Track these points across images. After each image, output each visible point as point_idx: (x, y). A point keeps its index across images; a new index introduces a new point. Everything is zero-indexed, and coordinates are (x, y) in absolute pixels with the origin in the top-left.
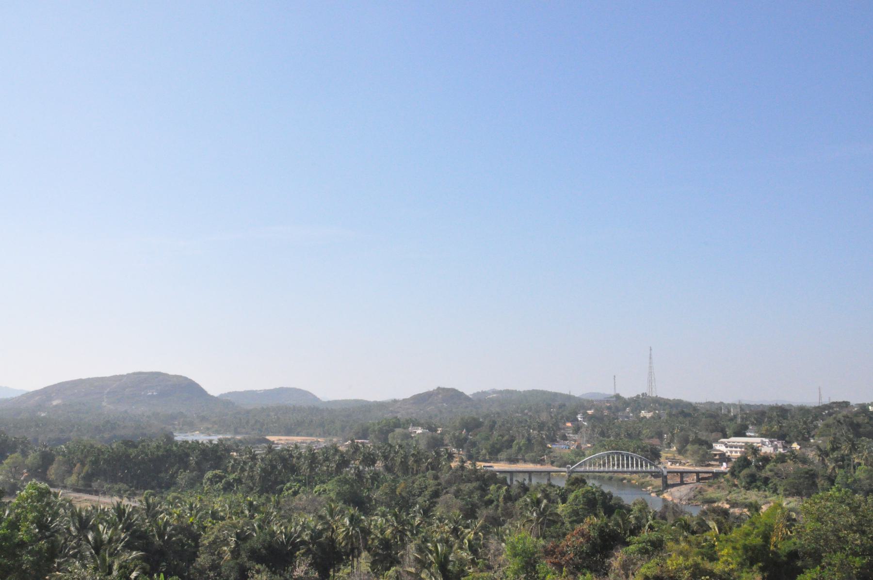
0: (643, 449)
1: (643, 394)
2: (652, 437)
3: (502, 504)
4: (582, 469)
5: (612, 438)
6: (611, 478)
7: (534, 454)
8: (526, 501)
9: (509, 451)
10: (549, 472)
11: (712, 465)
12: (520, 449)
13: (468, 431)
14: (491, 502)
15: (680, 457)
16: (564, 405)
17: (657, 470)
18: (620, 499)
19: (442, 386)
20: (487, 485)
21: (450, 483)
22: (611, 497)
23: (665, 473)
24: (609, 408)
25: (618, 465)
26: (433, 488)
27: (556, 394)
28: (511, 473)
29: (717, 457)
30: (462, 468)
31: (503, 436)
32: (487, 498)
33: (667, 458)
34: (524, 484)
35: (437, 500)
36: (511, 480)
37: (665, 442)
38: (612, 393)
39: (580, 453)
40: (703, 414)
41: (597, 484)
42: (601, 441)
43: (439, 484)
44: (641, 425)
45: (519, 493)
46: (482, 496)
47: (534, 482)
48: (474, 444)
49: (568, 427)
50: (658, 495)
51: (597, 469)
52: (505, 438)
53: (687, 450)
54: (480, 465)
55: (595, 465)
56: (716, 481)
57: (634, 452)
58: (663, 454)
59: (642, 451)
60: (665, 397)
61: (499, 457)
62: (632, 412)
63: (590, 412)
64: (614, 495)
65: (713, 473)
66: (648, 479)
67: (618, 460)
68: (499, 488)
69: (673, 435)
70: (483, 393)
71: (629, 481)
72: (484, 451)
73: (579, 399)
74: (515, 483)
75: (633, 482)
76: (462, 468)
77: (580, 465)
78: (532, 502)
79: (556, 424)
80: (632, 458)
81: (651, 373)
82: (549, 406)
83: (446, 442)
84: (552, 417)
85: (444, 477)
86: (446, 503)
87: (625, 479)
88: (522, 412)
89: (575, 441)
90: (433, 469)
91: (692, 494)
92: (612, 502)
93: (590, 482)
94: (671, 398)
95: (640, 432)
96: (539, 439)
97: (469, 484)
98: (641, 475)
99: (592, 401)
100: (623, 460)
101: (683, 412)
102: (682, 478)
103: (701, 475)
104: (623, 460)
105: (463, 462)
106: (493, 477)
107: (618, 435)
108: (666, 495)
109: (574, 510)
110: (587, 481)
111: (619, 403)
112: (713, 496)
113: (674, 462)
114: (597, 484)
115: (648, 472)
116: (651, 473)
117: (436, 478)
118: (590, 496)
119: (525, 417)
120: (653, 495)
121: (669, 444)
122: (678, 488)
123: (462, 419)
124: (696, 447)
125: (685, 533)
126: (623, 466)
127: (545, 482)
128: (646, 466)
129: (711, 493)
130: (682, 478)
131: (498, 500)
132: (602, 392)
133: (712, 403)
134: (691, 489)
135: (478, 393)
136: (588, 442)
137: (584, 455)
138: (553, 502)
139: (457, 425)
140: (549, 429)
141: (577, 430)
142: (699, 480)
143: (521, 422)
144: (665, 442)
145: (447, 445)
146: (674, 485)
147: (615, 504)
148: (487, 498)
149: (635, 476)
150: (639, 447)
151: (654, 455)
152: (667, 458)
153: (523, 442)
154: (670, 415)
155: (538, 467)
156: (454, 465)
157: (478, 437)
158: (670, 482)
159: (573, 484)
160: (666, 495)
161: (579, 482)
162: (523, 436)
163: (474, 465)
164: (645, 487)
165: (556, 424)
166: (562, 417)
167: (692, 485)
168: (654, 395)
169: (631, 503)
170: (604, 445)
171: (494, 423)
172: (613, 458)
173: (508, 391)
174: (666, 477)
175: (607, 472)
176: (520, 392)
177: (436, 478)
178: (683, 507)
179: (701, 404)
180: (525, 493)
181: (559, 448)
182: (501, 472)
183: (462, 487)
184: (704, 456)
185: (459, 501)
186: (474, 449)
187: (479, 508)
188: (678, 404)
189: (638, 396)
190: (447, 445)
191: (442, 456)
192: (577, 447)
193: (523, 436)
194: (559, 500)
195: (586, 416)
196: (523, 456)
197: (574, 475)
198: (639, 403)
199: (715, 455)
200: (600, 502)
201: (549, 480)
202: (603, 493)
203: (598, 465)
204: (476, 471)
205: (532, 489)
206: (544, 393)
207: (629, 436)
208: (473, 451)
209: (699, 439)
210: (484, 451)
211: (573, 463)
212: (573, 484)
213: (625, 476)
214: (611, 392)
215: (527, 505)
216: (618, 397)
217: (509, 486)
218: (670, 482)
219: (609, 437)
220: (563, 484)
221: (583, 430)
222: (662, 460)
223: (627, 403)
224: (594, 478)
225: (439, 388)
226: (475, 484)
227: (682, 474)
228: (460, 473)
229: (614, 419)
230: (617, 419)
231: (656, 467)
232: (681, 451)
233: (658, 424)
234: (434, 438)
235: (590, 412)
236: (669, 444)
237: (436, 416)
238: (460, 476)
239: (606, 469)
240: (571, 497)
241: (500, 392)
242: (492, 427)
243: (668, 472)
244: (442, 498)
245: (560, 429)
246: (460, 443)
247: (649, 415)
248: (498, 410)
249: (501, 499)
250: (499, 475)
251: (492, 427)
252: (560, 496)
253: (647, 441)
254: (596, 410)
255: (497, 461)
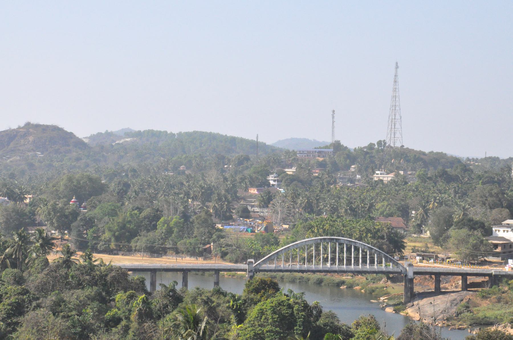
0: (376, 235)
1: (379, 143)
2: (391, 215)
3: (134, 325)
4: (273, 266)
5: (324, 216)
6: (319, 282)
7: (192, 241)
8: (176, 319)
9: (151, 234)
10: (217, 271)
11: (490, 263)
12: (170, 231)
13: (80, 200)
14: (116, 321)
15: (437, 248)
16: (247, 159)
17: (396, 269)
18: (333, 316)
19: (34, 121)
20: (109, 293)
21: (44, 289)
22: (320, 312)
23: (410, 275)
24: (322, 165)
25: (333, 260)
26: (13, 299)
27: (233, 140)
28: (154, 271)
29: (499, 250)
30: (67, 263)
31: (140, 210)
32: (109, 314)
33: (414, 250)
34: (173, 290)
35: (21, 319)
36: (153, 284)
37: (413, 222)
38: (329, 140)
39: (270, 239)
40: (480, 177)
41: (297, 291)
42: (306, 220)
43: (26, 292)
44: (373, 194)
45: (166, 306)
46: (101, 312)
47: (192, 287)
48: (89, 223)
49: (251, 196)
50: (397, 311)
51: (298, 267)
52: (147, 212)
53: (448, 237)
54: (98, 258)
55: (293, 260)
56: (495, 288)
57: (360, 239)
58: (409, 244)
59: (373, 237)
60: (417, 148)
61: (133, 244)
62: (360, 171)
63: (290, 171)
64: (325, 310)
65: (490, 275)
66: (381, 283)
67: (334, 252)
68: (132, 297)
69: (426, 211)
70: (109, 134)
71: (350, 287)
72: (107, 235)
73: (272, 149)
74: (158, 288)
75: (357, 288)
76: (67, 263)
77: (270, 260)
78: (187, 321)
79: (232, 191)
80: (357, 249)
81: (394, 108)
82: (221, 160)
83: (40, 217)
84: (225, 179)
85: (35, 278)
86: (37, 324)
87: (343, 283)
88: (175, 169)
89: (263, 219)
90: (14, 265)
91: (454, 310)
92: (321, 322)
93: (285, 288)
94: (427, 151)
95: (372, 206)
96: (203, 214)
97: (79, 291)
98: (370, 277)
99: (294, 153)
100: (342, 251)
101: (446, 172)
102: (438, 282)
103: (471, 280)
104: (342, 251)
105: (69, 253)
106: (120, 278)
107: (334, 210)
108: (411, 312)
109: (256, 335)
110: (281, 286)
111: (338, 157)
112: (489, 314)
113: (425, 256)
114: (297, 291)
115: (382, 272)
116: (386, 273)
117: (19, 281)
118: (285, 311)
119: (181, 178)
120: (389, 310)
121: (419, 226)
122: (431, 299)
123: (70, 179)
124: (465, 231)
125: (396, 238)
126: (341, 261)
127: (210, 287)
128: (380, 262)
129: (486, 309)
130: (438, 282)
131: (128, 318)
132: (311, 138)
133: (494, 160)
134: (452, 302)
135: (99, 134)
136: (284, 221)
137: (277, 243)
138: (222, 321)
139: (62, 188)
140: (220, 199)
141: (267, 201)
142: (466, 287)
143: (172, 187)
144: (413, 222)
145: (41, 224)
146: (423, 295)
147: (325, 325)
148: (109, 314)
149: (361, 279)
150: (368, 231)
151: (395, 244)
152: (414, 250)
153: (175, 219)
154: (424, 178)
155: (199, 263)
156: (52, 257)
157: (97, 211)
158: (417, 289)
159: (257, 291)
160: (411, 312)
161: (268, 287)
162: (176, 210)
163: (89, 257)
164: (377, 297)
165: (232, 191)
166: (243, 180)
167: (453, 296)
168: (398, 145)
169: (352, 324)
170: (311, 227)
171: (127, 186)
172: (325, 249)
173: (152, 134)
174: (411, 281)
175: (314, 272)
176: (173, 135)
177: (19, 281)
178: (438, 331)
179: (476, 160)
180: (175, 306)
181: (235, 231)
182: (135, 270)
183: (67, 296)
184: (476, 247)
185: (59, 320)
186: (90, 232)
187: (94, 332)
188: (437, 160)
189: (371, 146)
190: (41, 224)
191: (32, 243)
192: (266, 229)
193: (176, 210)
194: (233, 317)
195: (282, 178)
196: (175, 243)
197: (259, 276)
198: (373, 157)
199: (496, 246)
200: (299, 321)
201: (217, 283)
202: (306, 306)
203: (296, 260)
204: (92, 268)
205: (187, 299)
206: (212, 137)
207: (354, 212)
208: (89, 234)
209: (471, 220)
210: (107, 235)
211: (258, 256)
212: (257, 291)
213: (344, 278)
214: (324, 137)
215: (177, 326)
216: (337, 146)
217: (149, 294)
218: (417, 289)
219: (319, 213)
220: (240, 291)
221: (277, 201)
222: (406, 252)
223: (351, 157)
224: (293, 281)
225: (28, 125)
226: (90, 291)
227: (438, 276)
228: (63, 271)
229: (329, 183)
230: (335, 182)
231: (396, 264)
232: (439, 239)
233: (402, 193)
234: (20, 214)
235: (290, 171)
236: (419, 226)
237: (23, 172)
238: (63, 277)
239: (313, 267)
240: (253, 312)
241: (139, 134)
242: (122, 194)
243: (415, 273)
244: (30, 315)
245: (238, 199)
246: (65, 221)
247: (387, 178)
248: (134, 165)
249: (134, 316)
250: (132, 277)
251: (122, 194)
252: (235, 311)
253: (383, 221)
254: (300, 167)
255: (129, 251)
